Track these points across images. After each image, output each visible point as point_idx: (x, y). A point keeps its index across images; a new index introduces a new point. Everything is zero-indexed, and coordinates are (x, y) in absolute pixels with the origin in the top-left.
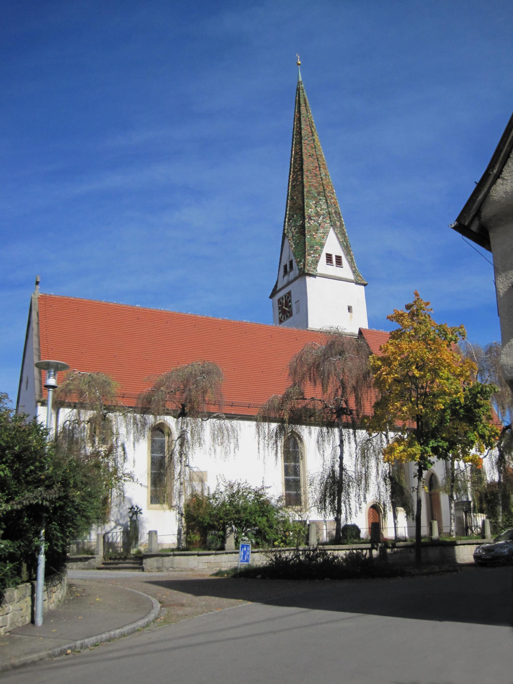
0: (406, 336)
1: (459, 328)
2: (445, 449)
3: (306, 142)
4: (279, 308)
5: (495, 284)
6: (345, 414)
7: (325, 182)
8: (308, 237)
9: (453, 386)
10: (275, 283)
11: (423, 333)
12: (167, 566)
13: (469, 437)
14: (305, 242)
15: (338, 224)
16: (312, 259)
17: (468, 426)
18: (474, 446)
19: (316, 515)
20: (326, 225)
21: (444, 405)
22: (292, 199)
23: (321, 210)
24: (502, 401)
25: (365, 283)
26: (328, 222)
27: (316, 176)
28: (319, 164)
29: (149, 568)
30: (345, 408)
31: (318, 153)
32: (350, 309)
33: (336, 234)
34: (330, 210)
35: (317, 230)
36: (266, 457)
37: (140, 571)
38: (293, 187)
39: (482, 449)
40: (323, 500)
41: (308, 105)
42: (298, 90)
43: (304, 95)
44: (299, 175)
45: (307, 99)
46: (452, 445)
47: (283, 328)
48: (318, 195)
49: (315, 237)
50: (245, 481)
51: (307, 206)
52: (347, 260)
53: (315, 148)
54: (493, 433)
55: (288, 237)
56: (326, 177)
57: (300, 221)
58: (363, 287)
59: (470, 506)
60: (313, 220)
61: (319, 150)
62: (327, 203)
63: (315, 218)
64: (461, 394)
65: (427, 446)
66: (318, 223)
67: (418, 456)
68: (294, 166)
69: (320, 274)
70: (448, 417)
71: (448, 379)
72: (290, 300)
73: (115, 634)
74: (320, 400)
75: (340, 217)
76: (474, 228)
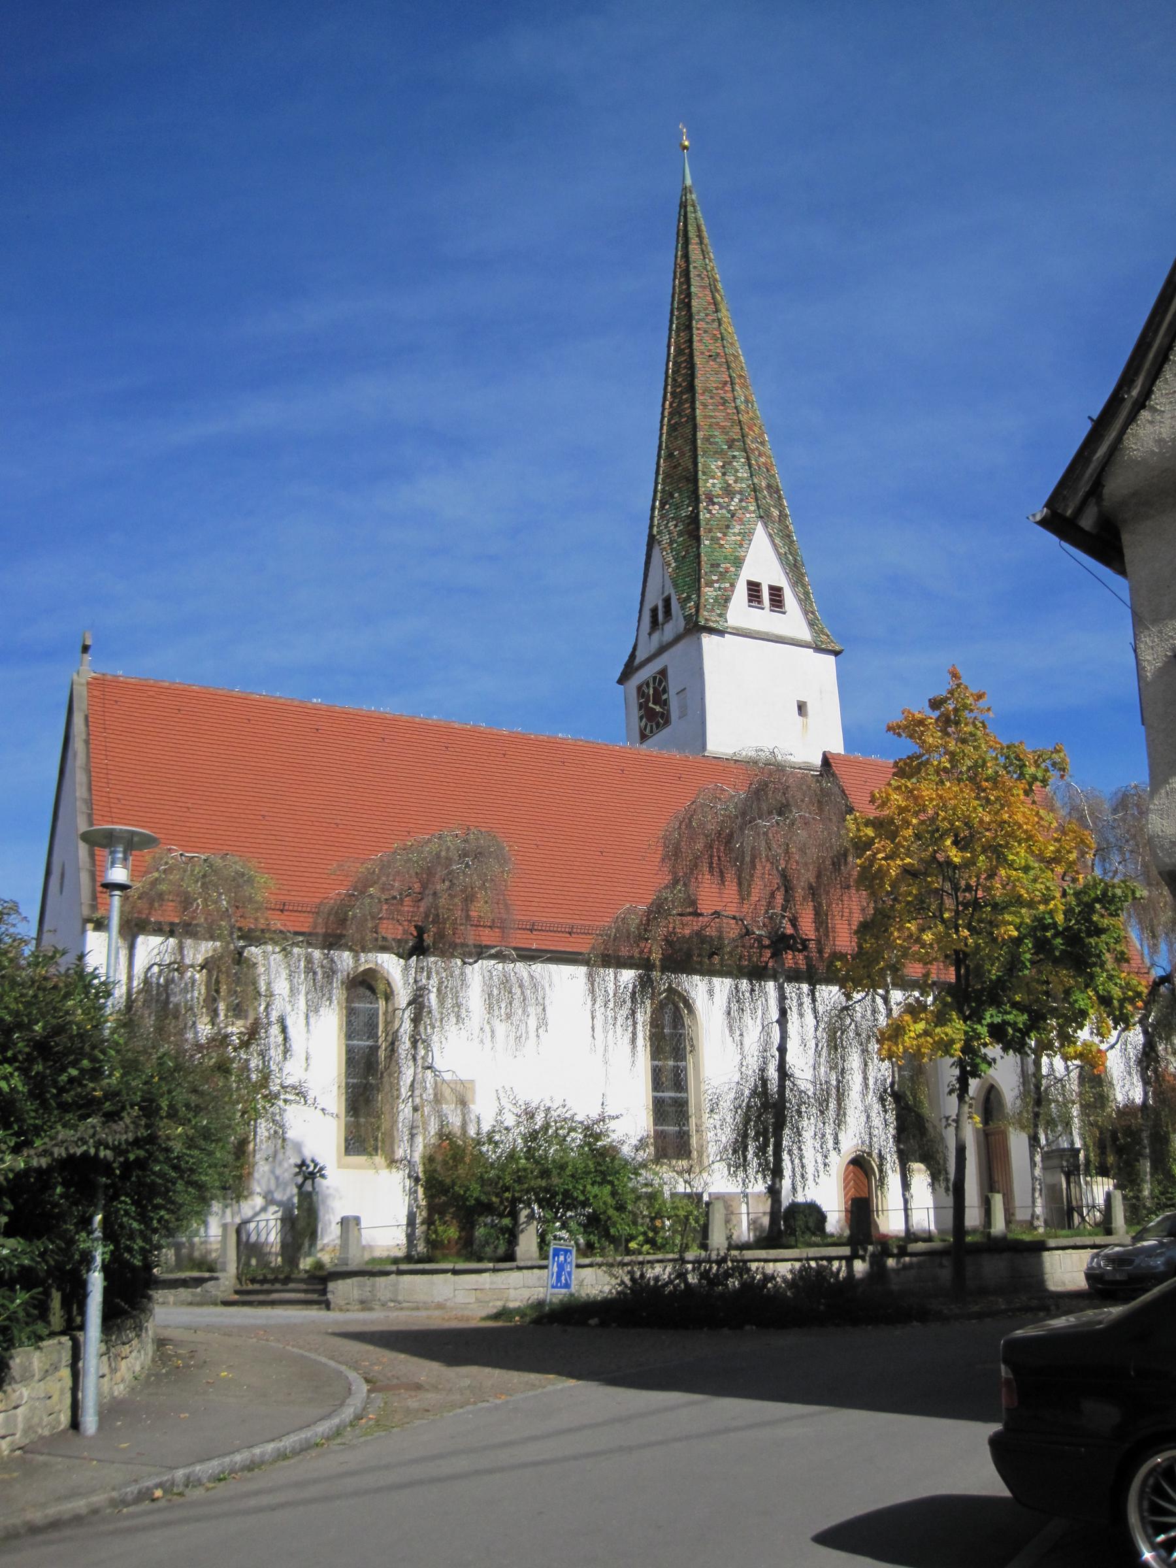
0: (931, 770)
1: (1052, 753)
2: (1020, 1030)
3: (702, 325)
4: (641, 706)
5: (1135, 651)
6: (793, 948)
7: (744, 418)
8: (707, 542)
9: (1038, 886)
10: (630, 650)
11: (969, 763)
12: (382, 1298)
13: (1076, 1001)
14: (698, 556)
15: (775, 513)
16: (715, 593)
17: (1074, 977)
18: (1087, 1023)
19: (724, 1180)
20: (748, 515)
21: (1017, 929)
22: (670, 455)
23: (736, 482)
24: (1151, 920)
25: (837, 648)
26: (752, 508)
27: (723, 404)
28: (730, 377)
29: (342, 1303)
30: (791, 936)
31: (729, 351)
32: (802, 708)
33: (770, 536)
34: (756, 481)
35: (728, 527)
36: (610, 1049)
37: (320, 1309)
38: (673, 428)
39: (1104, 1030)
40: (739, 1147)
41: (706, 241)
42: (683, 205)
43: (696, 219)
44: (686, 400)
45: (703, 228)
46: (1036, 1020)
47: (648, 753)
48: (730, 447)
49: (722, 542)
50: (561, 1103)
51: (704, 473)
52: (796, 595)
53: (722, 340)
54: (1130, 993)
55: (659, 542)
56: (747, 407)
57: (688, 506)
58: (832, 658)
59: (1078, 1160)
60: (719, 504)
61: (732, 344)
62: (750, 466)
63: (721, 500)
64: (1057, 904)
65: (979, 1022)
66: (729, 511)
67: (958, 1046)
68: (674, 380)
69: (734, 628)
70: (1028, 956)
71: (1026, 869)
72: (664, 687)
73: (263, 1454)
74: (734, 918)
75: (780, 498)
76: (1087, 522)
